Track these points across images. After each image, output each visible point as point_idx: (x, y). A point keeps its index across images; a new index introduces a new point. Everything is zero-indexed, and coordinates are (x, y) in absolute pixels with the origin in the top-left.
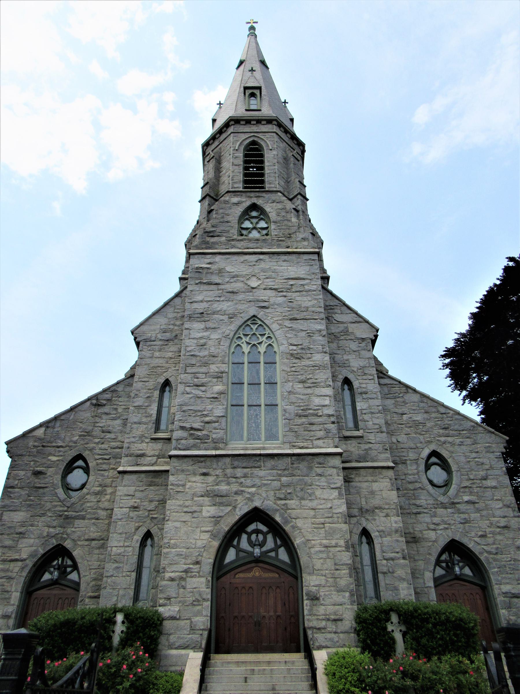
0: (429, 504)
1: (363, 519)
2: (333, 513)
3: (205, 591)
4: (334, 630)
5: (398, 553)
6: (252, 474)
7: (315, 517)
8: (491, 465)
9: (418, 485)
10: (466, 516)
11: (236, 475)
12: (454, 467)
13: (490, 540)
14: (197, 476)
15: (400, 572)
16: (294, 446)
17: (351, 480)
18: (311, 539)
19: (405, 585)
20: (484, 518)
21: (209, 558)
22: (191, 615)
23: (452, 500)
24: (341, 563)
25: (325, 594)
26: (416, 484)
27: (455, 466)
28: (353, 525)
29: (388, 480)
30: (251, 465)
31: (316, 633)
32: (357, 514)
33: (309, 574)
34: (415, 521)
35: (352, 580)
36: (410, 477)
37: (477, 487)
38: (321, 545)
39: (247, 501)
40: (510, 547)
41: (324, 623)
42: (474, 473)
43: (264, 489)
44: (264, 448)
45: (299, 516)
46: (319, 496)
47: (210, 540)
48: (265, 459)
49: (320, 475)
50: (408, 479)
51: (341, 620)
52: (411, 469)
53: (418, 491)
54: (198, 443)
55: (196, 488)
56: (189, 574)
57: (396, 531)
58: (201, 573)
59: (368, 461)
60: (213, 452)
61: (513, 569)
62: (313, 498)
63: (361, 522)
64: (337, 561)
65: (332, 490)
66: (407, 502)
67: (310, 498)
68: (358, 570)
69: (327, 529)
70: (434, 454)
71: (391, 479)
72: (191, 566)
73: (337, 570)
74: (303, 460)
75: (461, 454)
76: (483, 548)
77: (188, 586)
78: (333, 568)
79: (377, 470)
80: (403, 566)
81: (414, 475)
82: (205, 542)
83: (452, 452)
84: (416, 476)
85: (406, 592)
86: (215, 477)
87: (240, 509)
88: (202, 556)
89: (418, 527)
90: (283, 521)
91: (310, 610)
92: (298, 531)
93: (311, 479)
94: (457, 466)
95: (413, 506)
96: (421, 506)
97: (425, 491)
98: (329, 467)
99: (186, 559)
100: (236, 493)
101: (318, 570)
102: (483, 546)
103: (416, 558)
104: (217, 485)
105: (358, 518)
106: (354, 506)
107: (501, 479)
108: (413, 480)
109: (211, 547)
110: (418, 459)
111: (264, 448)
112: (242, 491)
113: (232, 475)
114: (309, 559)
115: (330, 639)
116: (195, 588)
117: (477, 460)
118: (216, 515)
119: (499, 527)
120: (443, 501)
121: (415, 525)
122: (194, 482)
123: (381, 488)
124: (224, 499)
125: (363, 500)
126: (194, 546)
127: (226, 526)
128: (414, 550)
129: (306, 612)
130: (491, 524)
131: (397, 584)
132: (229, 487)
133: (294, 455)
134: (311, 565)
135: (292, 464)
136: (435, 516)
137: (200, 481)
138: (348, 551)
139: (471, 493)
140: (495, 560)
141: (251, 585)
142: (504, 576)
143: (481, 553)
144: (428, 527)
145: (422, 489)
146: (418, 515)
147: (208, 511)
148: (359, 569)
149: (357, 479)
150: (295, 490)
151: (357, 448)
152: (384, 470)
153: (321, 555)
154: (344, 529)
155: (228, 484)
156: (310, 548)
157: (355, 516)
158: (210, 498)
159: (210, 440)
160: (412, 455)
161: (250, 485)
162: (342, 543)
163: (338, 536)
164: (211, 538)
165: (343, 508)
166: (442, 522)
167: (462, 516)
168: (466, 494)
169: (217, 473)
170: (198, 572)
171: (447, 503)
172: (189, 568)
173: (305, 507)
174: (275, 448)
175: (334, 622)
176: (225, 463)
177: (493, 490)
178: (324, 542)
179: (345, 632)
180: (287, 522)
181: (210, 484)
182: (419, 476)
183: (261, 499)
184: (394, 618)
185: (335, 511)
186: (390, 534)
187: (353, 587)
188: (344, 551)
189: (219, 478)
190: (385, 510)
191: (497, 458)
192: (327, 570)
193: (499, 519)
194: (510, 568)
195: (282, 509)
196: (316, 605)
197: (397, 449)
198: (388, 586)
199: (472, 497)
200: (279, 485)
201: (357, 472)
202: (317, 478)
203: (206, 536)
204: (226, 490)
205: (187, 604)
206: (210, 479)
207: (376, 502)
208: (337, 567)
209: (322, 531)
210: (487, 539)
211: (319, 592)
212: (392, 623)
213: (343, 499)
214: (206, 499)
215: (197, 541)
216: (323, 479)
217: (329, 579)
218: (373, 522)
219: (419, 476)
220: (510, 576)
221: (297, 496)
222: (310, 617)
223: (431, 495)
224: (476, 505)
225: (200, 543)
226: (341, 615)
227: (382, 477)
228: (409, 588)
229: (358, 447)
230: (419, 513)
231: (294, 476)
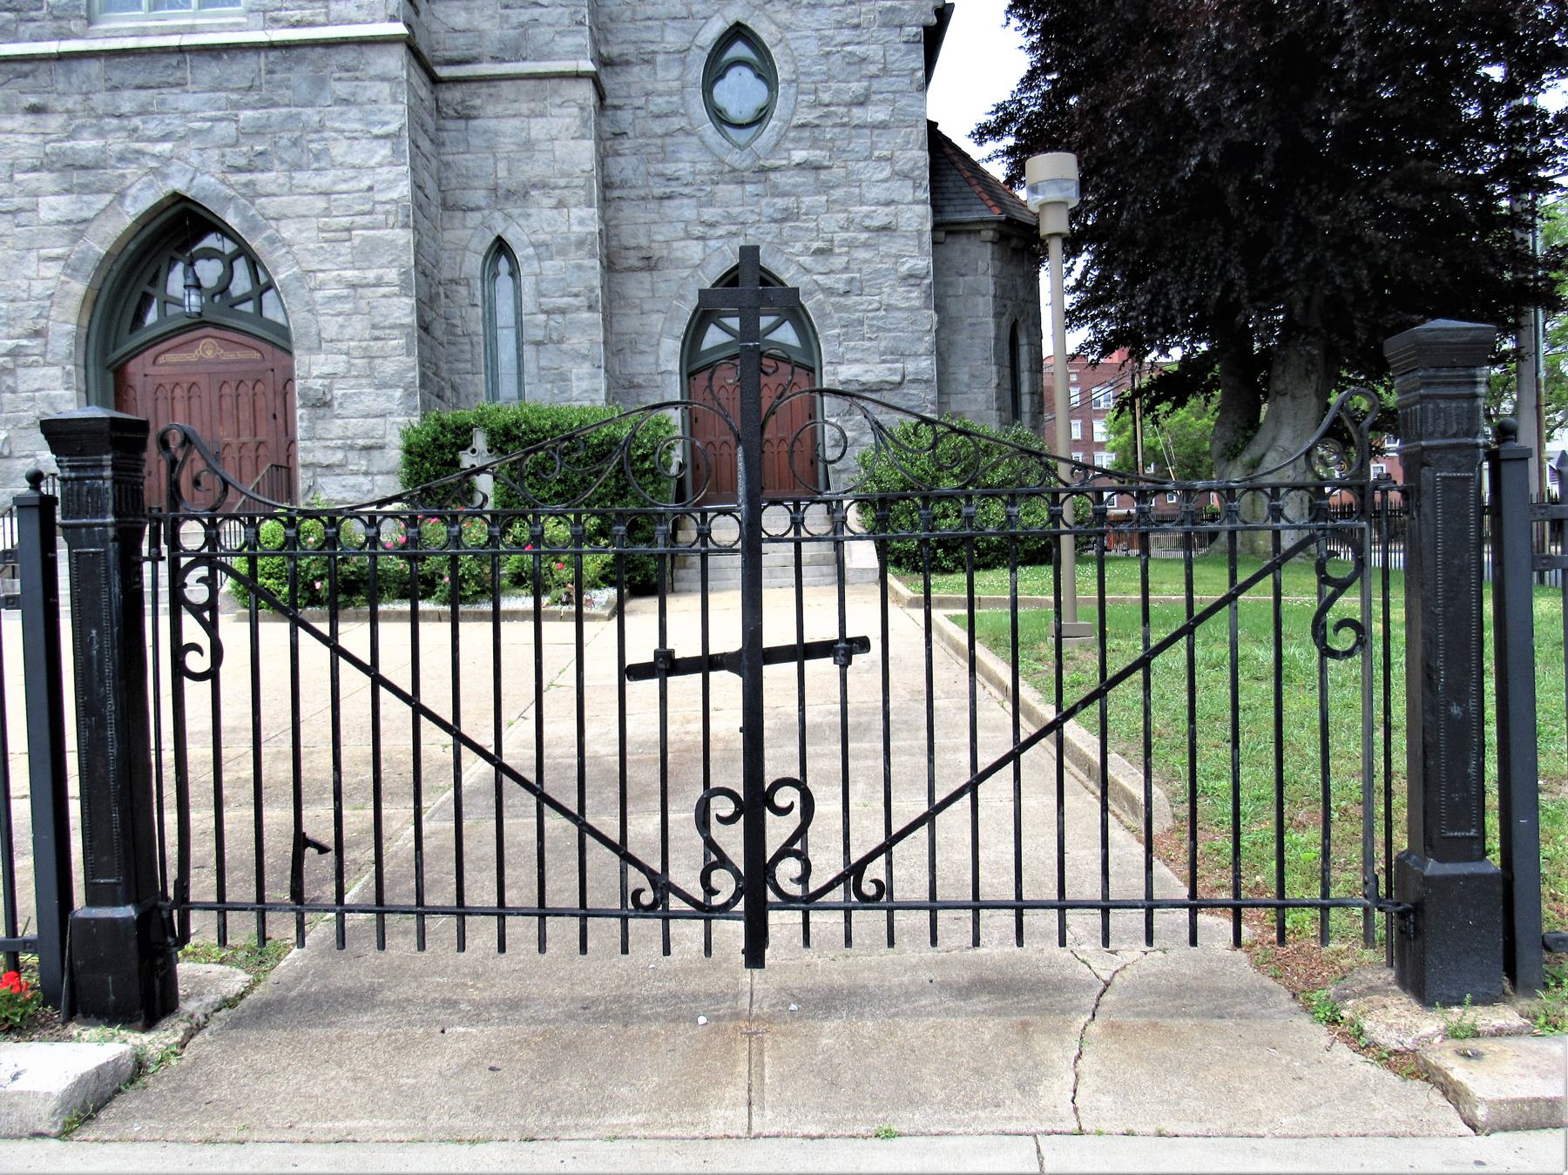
0: (701, 173)
1: (497, 214)
2: (375, 203)
3: (62, 397)
4: (364, 468)
5: (576, 295)
6: (163, 103)
7: (327, 213)
8: (885, 63)
9: (677, 122)
10: (790, 202)
11: (118, 108)
12: (784, 71)
13: (838, 262)
14: (18, 116)
15: (577, 341)
16: (276, 20)
17: (475, 113)
18: (314, 268)
19: (586, 368)
20: (837, 207)
21: (66, 322)
22: (35, 447)
23: (761, 162)
24: (387, 324)
25: (344, 395)
26: (671, 119)
27: (786, 68)
28: (471, 231)
29: (575, 111)
30: (156, 78)
31: (322, 475)
32: (483, 203)
33: (310, 350)
34: (655, 217)
35: (413, 361)
36: (660, 100)
37: (834, 126)
38: (339, 282)
39: (151, 177)
40: (884, 276)
41: (339, 455)
42: (834, 85)
43: (193, 144)
44: (192, 30)
45: (288, 212)
46: (340, 159)
47: (63, 278)
48: (198, 61)
49: (346, 102)
50: (652, 107)
51: (381, 448)
52: (667, 76)
53: (675, 140)
54: (9, 21)
55: (17, 148)
56: (22, 360)
57: (580, 244)
58: (49, 356)
59: (524, 59)
60: (52, 47)
61: (879, 329)
62: (323, 164)
63: (492, 222)
64: (378, 319)
65: (375, 143)
66: (642, 168)
67: (316, 165)
68: (475, 339)
69: (356, 242)
70: (738, 32)
71: (582, 109)
72: (24, 342)
73: (377, 339)
74: (299, 61)
75: (809, 33)
76: (816, 282)
77: (22, 387)
78: (367, 336)
79: (547, 84)
80: (585, 328)
81: (670, 94)
82: (51, 283)
83: (787, 28)
84: (675, 99)
85: (585, 385)
86: (65, 115)
87: (135, 199)
88: (47, 318)
89: (662, 233)
90: (246, 226)
91: (311, 428)
92: (284, 250)
93: (319, 112)
94: (792, 68)
95: (656, 179)
96: (677, 179)
97: (695, 139)
98: (372, 79)
99: (10, 326)
100: (122, 159)
101: (331, 341)
102: (815, 277)
103: (647, 307)
104: (70, 137)
105: (486, 212)
106: (476, 183)
107: (903, 102)
108: (666, 108)
109: (67, 294)
110: (688, 49)
111: (192, 30)
112: (137, 152)
113: (110, 109)
114: (309, 316)
115: (353, 486)
116: (39, 390)
117: (849, 48)
118: (75, 217)
119: (867, 229)
120: (737, 166)
121: (654, 228)
122: (11, 132)
123: (554, 133)
124: (88, 177)
125: (502, 165)
126: (25, 296)
127: (101, 243)
128: (643, 289)
129: (299, 433)
130: (850, 221)
131: (567, 365)
132: (102, 142)
133: (272, 46)
134: (314, 330)
135: (271, 72)
136: (710, 204)
137: (25, 130)
138: (406, 295)
139: (815, 143)
140: (839, 308)
141: (194, 379)
142: (852, 344)
143: (810, 294)
144: (686, 231)
145: (688, 134)
146: (666, 203)
147: (55, 206)
148: (478, 335)
149: (490, 109)
150: (275, 143)
151: (497, 20)
152: (565, 83)
153: (339, 307)
154: (402, 242)
155: (101, 133)
156: (312, 290)
157: (478, 209)
158: (54, 175)
159: (45, 11)
160: (673, 38)
161: (156, 133)
162: (392, 275)
163: (387, 258)
164: (66, 275)
165: (404, 189)
166: (724, 218)
167: (781, 202)
168: (802, 145)
169: (70, 105)
170: (43, 355)
171: (746, 170)
172: (18, 346)
173: (302, 191)
174: (223, 28)
175: (363, 453)
176: (88, 77)
177: (876, 132)
178: (349, 274)
179: (388, 473)
180: (255, 228)
181: (53, 137)
182: (683, 98)
183: (187, 171)
184: (480, 440)
185: (379, 197)
186: (562, 252)
187: (414, 375)
188: (395, 295)
189: (76, 117)
190: (557, 192)
191: (906, 42)
192: (352, 339)
193: (873, 208)
194: (871, 326)
195: (243, 195)
196: (323, 417)
197: (633, 20)
198: (543, 372)
199: (817, 152)
200: (233, 132)
201: (492, 90)
202: (336, 109)
203: (53, 270)
204: (95, 150)
205: (25, 424)
206: (53, 123)
207: (534, 170)
208: (377, 333)
209: (345, 248)
210: (833, 260)
211: (331, 391)
212: (474, 451)
213: (405, 164)
214: (45, 176)
215: (33, 283)
216: (354, 113)
217: (356, 361)
218: (522, 222)
219: (683, 98)
220: (867, 344)
221: (283, 162)
222: (308, 443)
223: (705, 146)
224: (823, 175)
225: (38, 288)
226: (382, 437)
227: (558, 101)
228: (593, 376)
229: (502, 16)
230: (670, 197)
231: (275, 105)
